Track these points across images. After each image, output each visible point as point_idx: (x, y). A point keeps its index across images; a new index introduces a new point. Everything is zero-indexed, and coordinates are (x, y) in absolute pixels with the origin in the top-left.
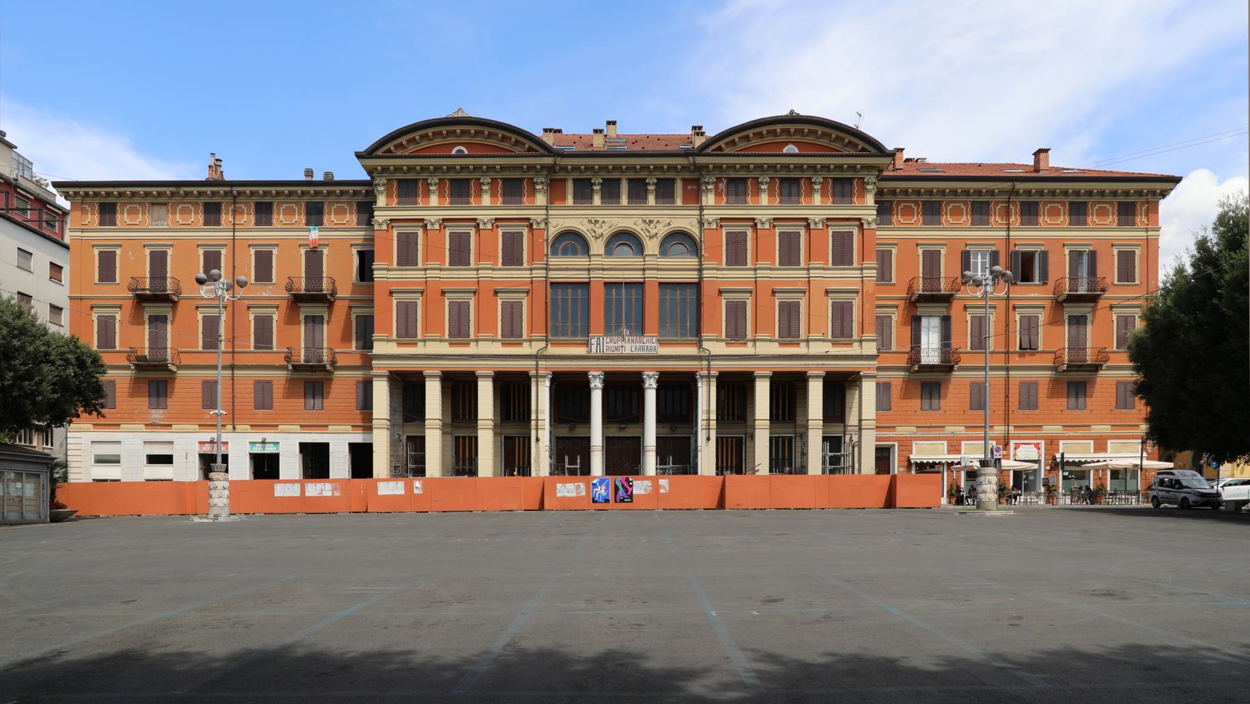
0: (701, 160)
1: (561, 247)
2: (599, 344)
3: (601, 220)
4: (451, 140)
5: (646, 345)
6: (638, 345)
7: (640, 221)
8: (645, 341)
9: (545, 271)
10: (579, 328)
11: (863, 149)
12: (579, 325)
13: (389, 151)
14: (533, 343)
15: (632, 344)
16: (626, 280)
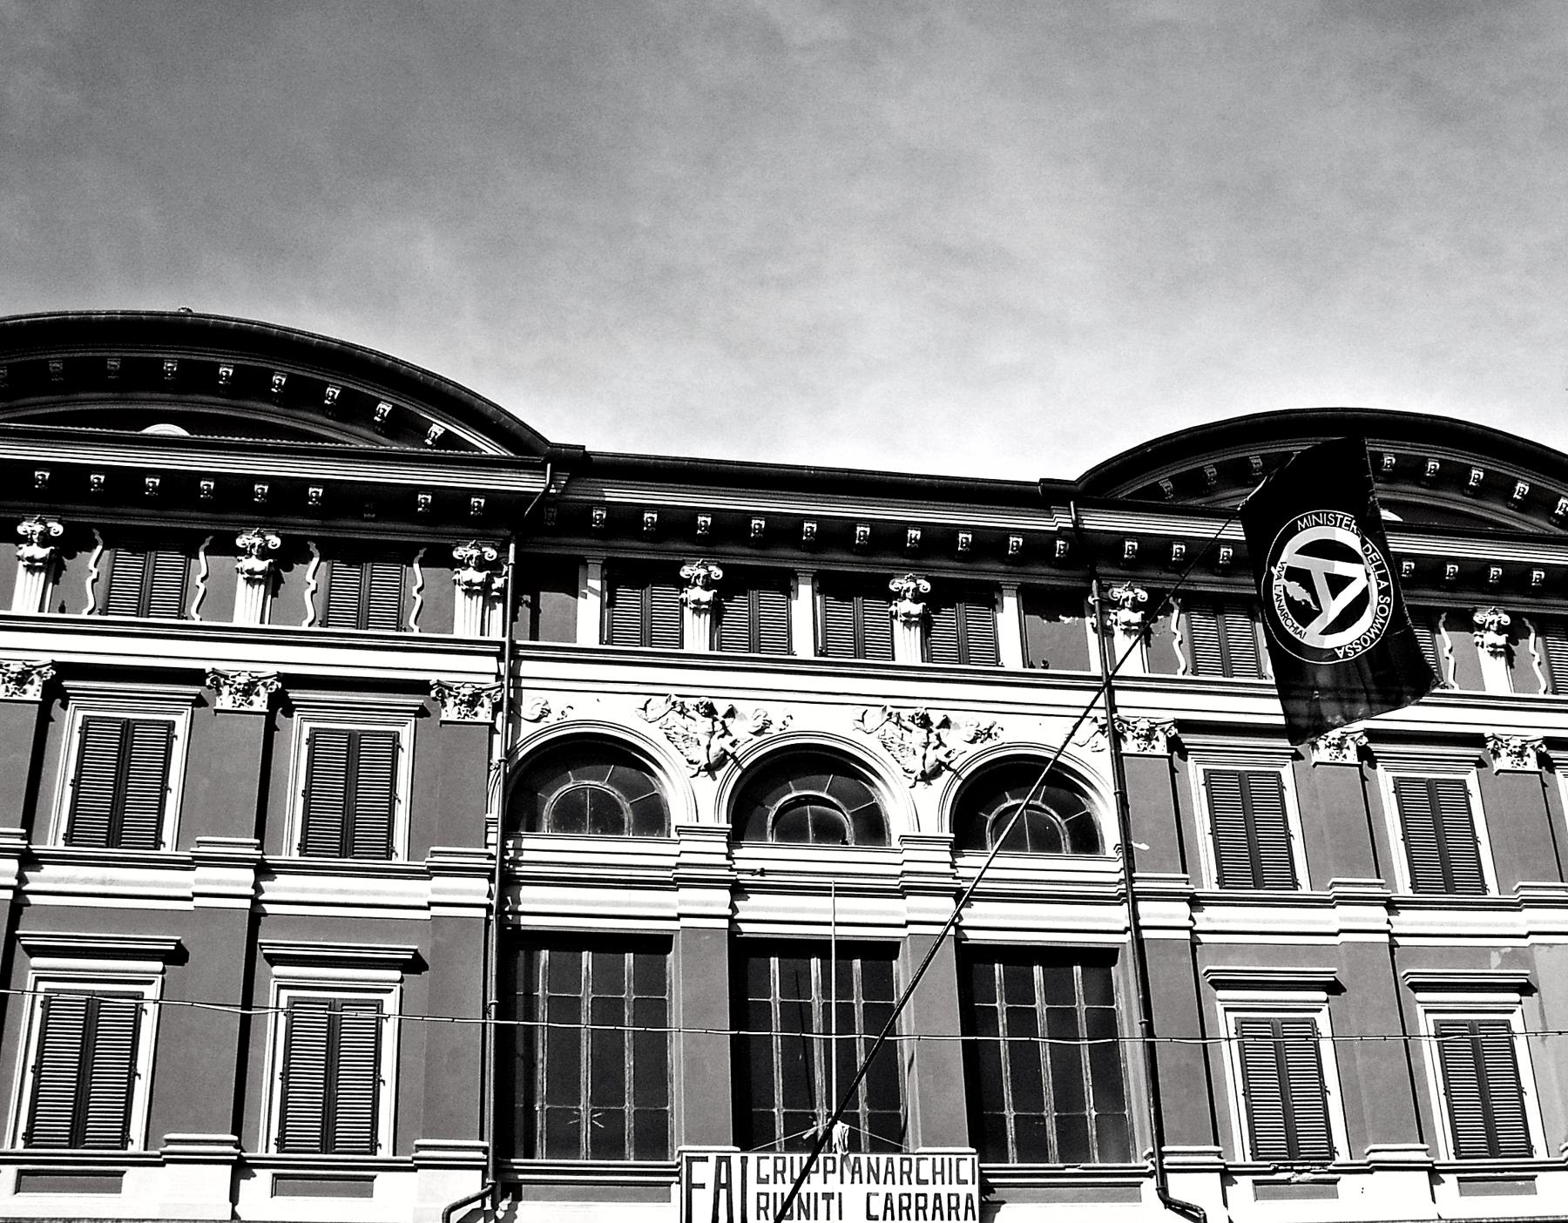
0: (1098, 521)
1: (626, 805)
2: (728, 1186)
3: (936, 718)
4: (144, 401)
5: (930, 1190)
6: (896, 1190)
7: (875, 717)
8: (926, 1173)
9: (949, 903)
10: (629, 1124)
11: (448, 440)
12: (629, 1107)
13: (1155, 491)
14: (695, 1181)
15: (873, 1187)
16: (841, 931)
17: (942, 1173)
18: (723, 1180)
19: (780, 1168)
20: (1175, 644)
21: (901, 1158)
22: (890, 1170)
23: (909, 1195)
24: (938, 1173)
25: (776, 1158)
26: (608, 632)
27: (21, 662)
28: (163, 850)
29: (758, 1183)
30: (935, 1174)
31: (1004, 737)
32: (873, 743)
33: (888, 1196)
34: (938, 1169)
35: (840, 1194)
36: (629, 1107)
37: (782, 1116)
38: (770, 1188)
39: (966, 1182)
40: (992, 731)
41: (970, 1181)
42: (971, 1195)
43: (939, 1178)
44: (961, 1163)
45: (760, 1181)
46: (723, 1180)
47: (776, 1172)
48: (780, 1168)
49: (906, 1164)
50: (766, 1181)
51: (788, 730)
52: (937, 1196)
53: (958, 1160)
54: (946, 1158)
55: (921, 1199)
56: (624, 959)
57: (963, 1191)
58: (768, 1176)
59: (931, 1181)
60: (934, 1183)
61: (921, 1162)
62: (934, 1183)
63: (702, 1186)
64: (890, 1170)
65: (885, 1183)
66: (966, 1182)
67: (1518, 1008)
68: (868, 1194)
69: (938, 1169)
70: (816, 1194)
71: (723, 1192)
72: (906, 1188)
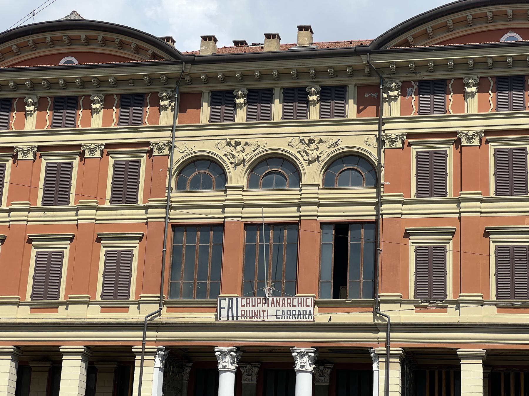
1: (190, 178)
2: (232, 308)
5: (297, 309)
6: (286, 309)
7: (296, 141)
8: (295, 303)
10: (208, 287)
12: (209, 281)
15: (278, 308)
16: (265, 219)
17: (301, 303)
18: (230, 306)
19: (248, 302)
20: (47, 116)
21: (287, 298)
22: (284, 302)
23: (290, 311)
24: (299, 303)
25: (247, 299)
26: (285, 116)
27: (26, 147)
28: (70, 205)
29: (241, 307)
30: (298, 303)
31: (341, 145)
32: (294, 151)
33: (283, 311)
34: (300, 302)
35: (267, 310)
36: (209, 281)
37: (256, 283)
38: (245, 308)
39: (309, 306)
40: (337, 143)
41: (310, 306)
42: (311, 310)
43: (300, 305)
44: (307, 300)
45: (242, 306)
46: (230, 306)
47: (247, 303)
48: (248, 302)
49: (289, 300)
50: (244, 306)
51: (193, 151)
52: (299, 311)
53: (306, 299)
54: (302, 298)
55: (294, 312)
56: (284, 232)
57: (308, 309)
58: (244, 305)
59: (297, 306)
60: (298, 307)
61: (307, 300)
62: (298, 307)
63: (224, 308)
64: (284, 302)
65: (282, 307)
66: (309, 306)
67: (452, 240)
68: (276, 310)
69: (300, 302)
70: (260, 310)
71: (230, 310)
72: (289, 308)
